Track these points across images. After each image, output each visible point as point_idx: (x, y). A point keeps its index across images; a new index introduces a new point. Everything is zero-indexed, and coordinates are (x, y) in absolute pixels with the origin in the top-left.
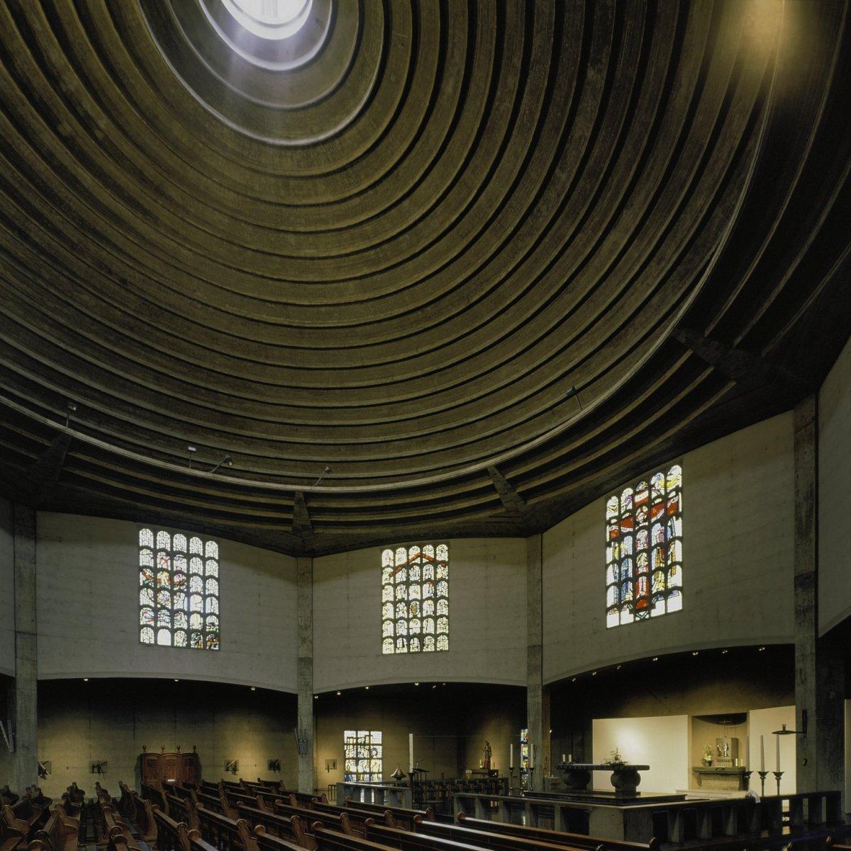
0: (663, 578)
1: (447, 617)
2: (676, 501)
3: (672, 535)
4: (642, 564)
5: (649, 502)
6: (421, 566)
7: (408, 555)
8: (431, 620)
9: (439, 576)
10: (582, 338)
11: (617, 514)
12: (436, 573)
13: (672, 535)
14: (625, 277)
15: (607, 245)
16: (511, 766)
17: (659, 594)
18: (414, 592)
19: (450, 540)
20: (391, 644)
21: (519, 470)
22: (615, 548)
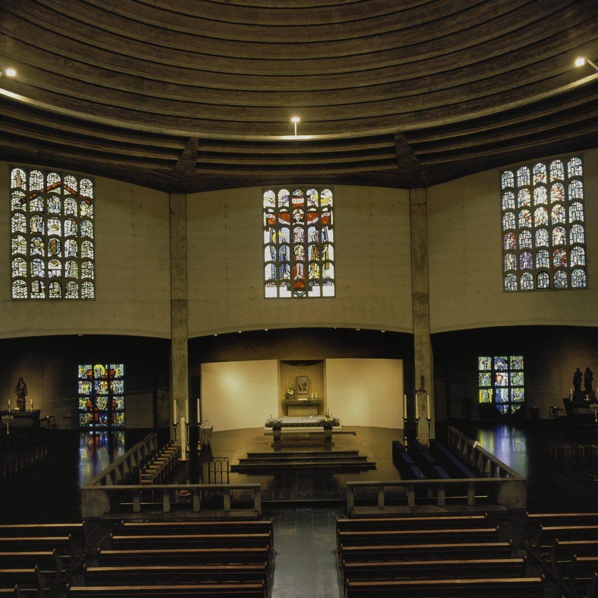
0: (318, 270)
1: (93, 261)
2: (329, 215)
3: (325, 239)
4: (300, 254)
5: (304, 207)
6: (62, 197)
7: (45, 182)
8: (74, 263)
9: (83, 213)
12: (79, 210)
13: (325, 239)
14: (351, 66)
16: (175, 423)
17: (314, 281)
18: (53, 228)
19: (96, 177)
20: (23, 286)
21: (215, 148)
22: (273, 233)
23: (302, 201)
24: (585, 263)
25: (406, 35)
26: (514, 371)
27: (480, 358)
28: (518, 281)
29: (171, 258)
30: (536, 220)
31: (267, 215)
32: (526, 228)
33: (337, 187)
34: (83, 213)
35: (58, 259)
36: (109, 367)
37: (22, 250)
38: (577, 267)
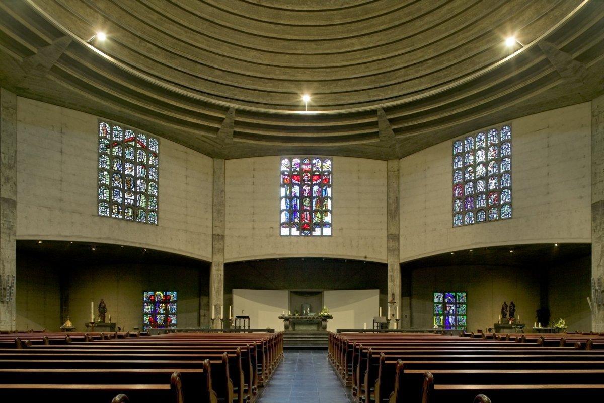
1: (157, 198)
3: (325, 194)
5: (311, 171)
6: (136, 149)
7: (124, 136)
9: (150, 162)
10: (308, 70)
11: (288, 170)
12: (148, 160)
14: (347, 61)
15: (348, 41)
16: (213, 318)
17: (317, 224)
20: (106, 207)
22: (288, 190)
23: (309, 167)
24: (511, 200)
25: (388, 34)
26: (459, 303)
27: (435, 294)
28: (463, 219)
29: (214, 205)
30: (478, 173)
31: (284, 177)
32: (470, 180)
33: (335, 158)
34: (150, 162)
35: (132, 192)
36: (166, 293)
37: (107, 181)
38: (505, 204)
